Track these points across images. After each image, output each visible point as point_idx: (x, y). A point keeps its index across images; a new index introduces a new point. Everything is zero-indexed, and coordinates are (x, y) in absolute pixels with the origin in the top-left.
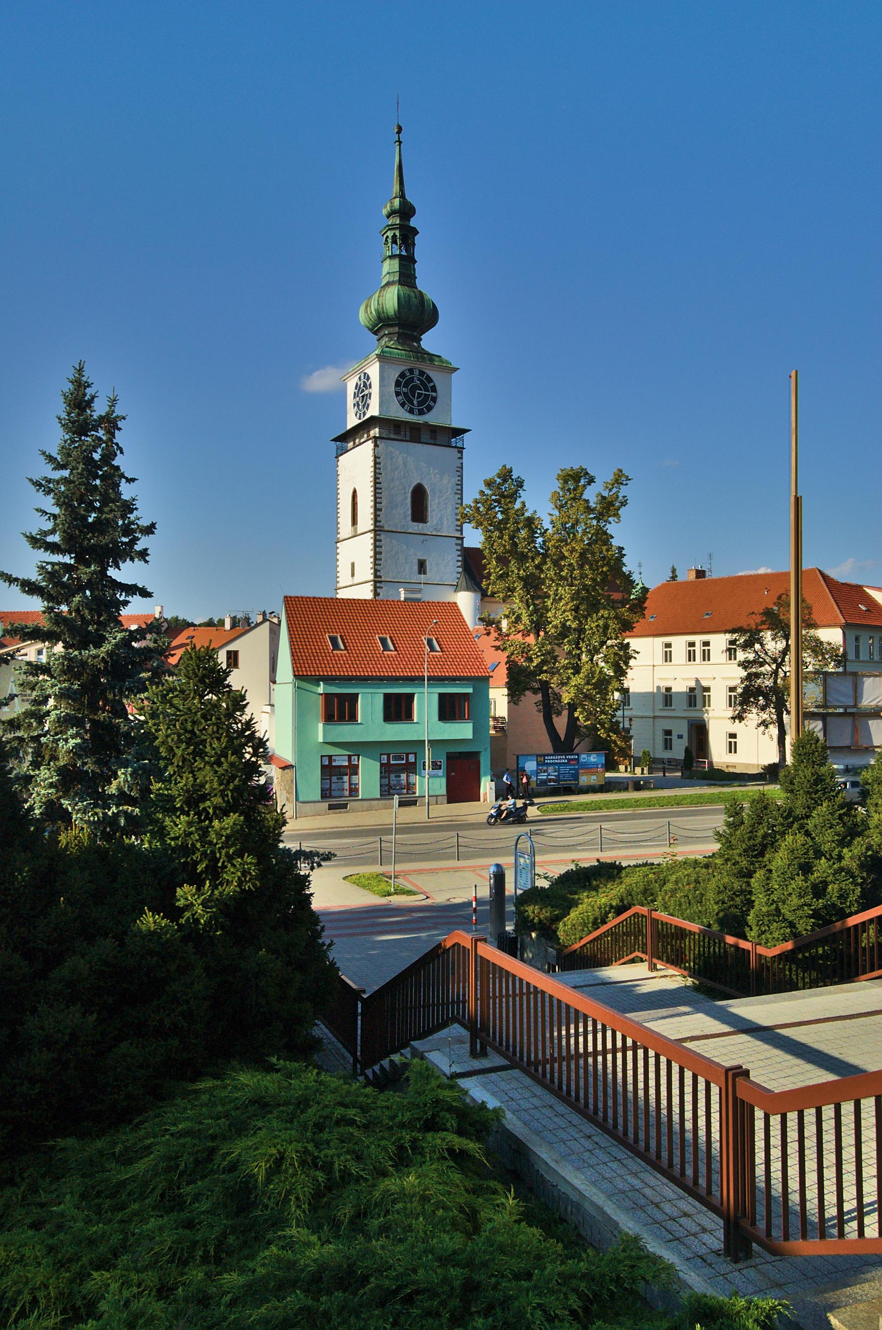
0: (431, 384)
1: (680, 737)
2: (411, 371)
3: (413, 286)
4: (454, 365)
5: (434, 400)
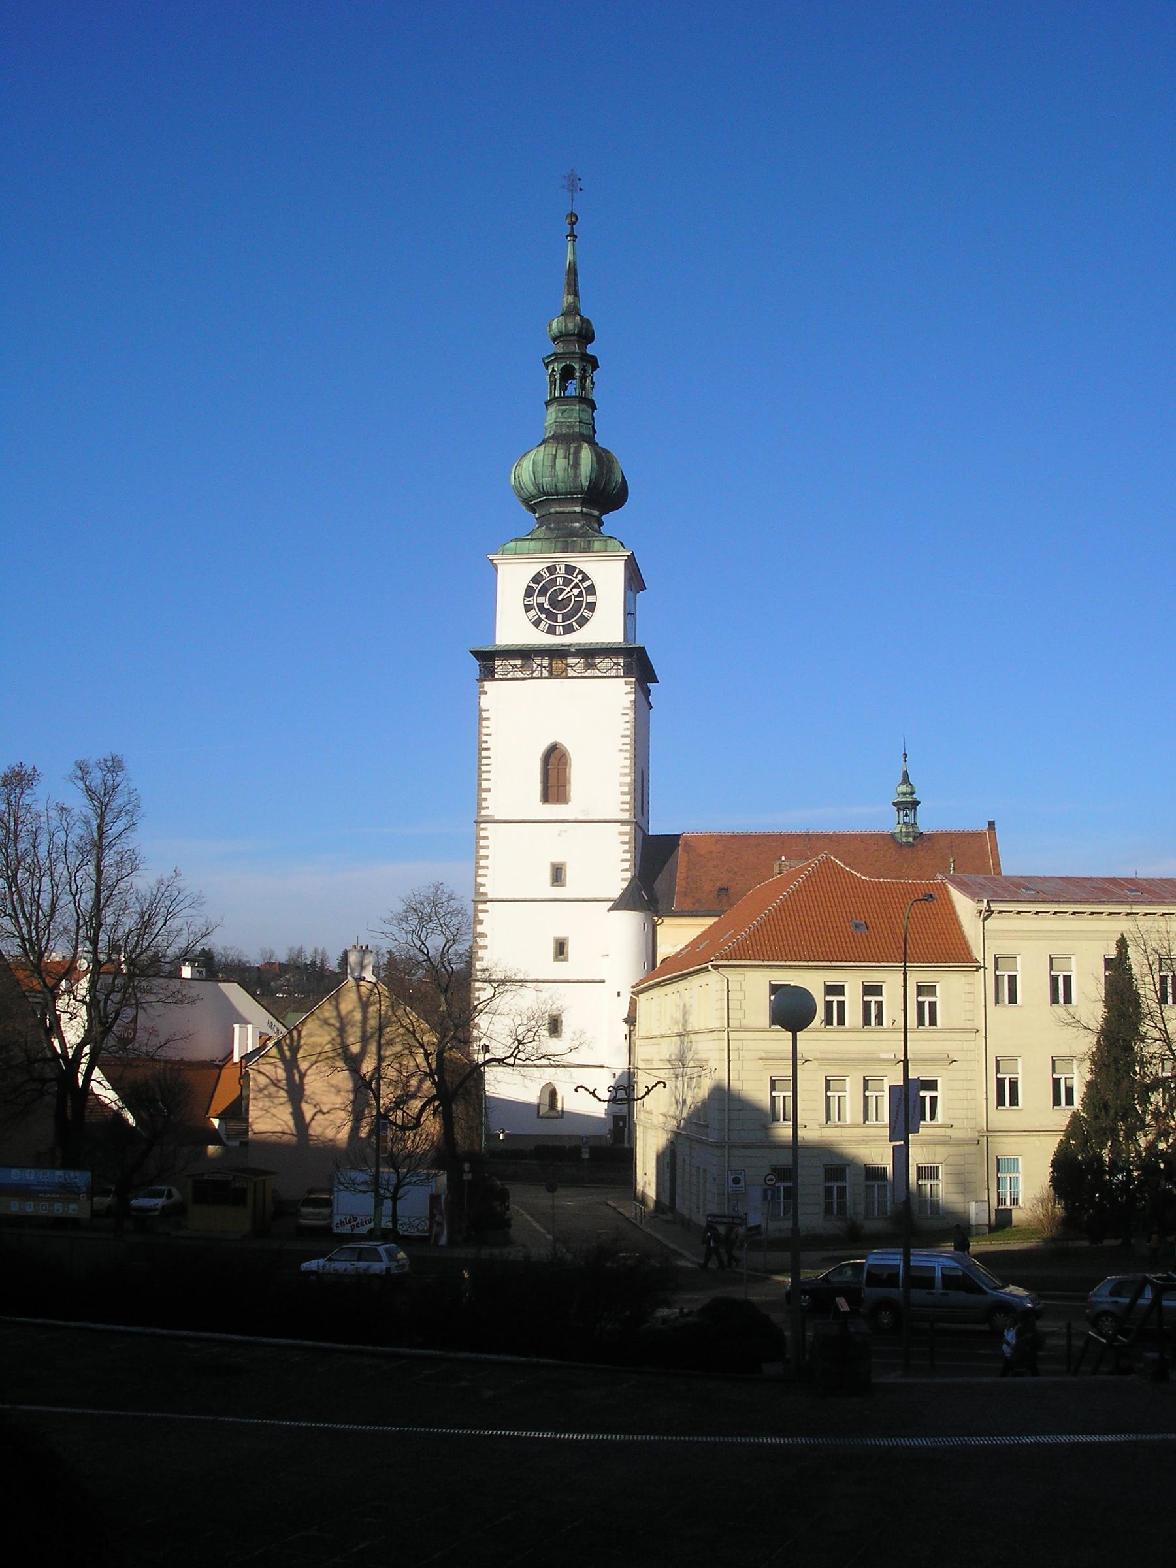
2: (551, 570)
5: (592, 607)
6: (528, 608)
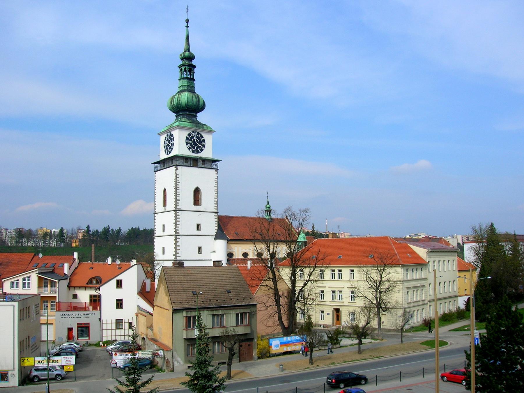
1: (328, 314)
3: (194, 92)
4: (213, 129)
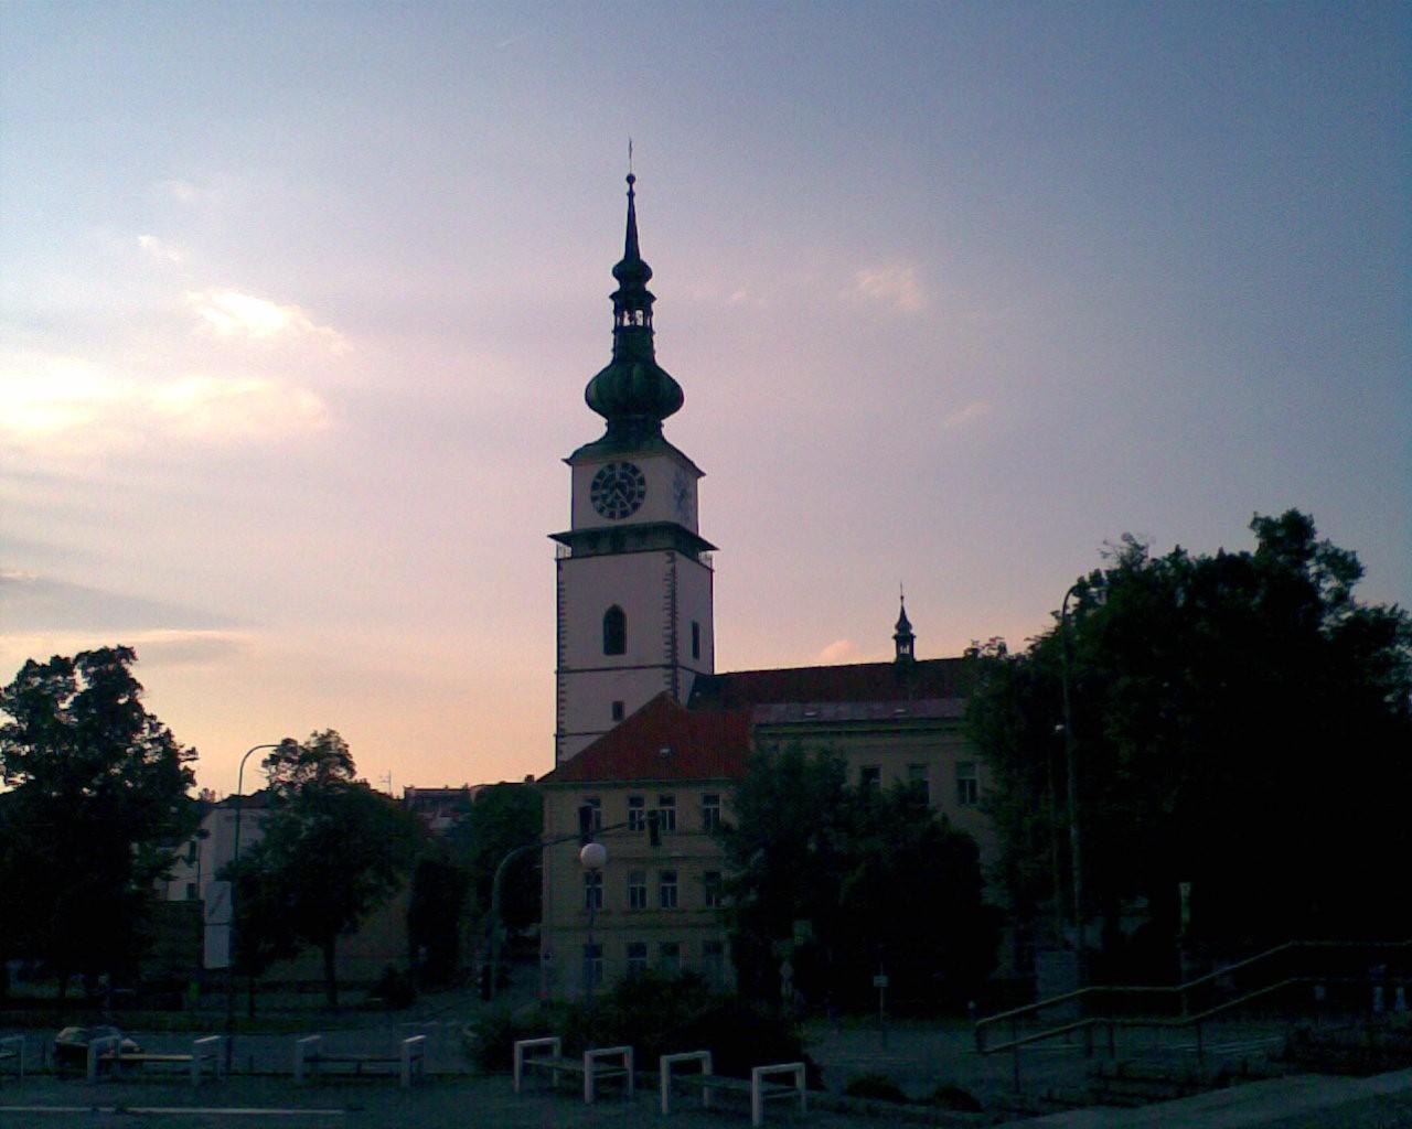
0: (598, 481)
2: (611, 467)
5: (642, 495)
6: (594, 499)
